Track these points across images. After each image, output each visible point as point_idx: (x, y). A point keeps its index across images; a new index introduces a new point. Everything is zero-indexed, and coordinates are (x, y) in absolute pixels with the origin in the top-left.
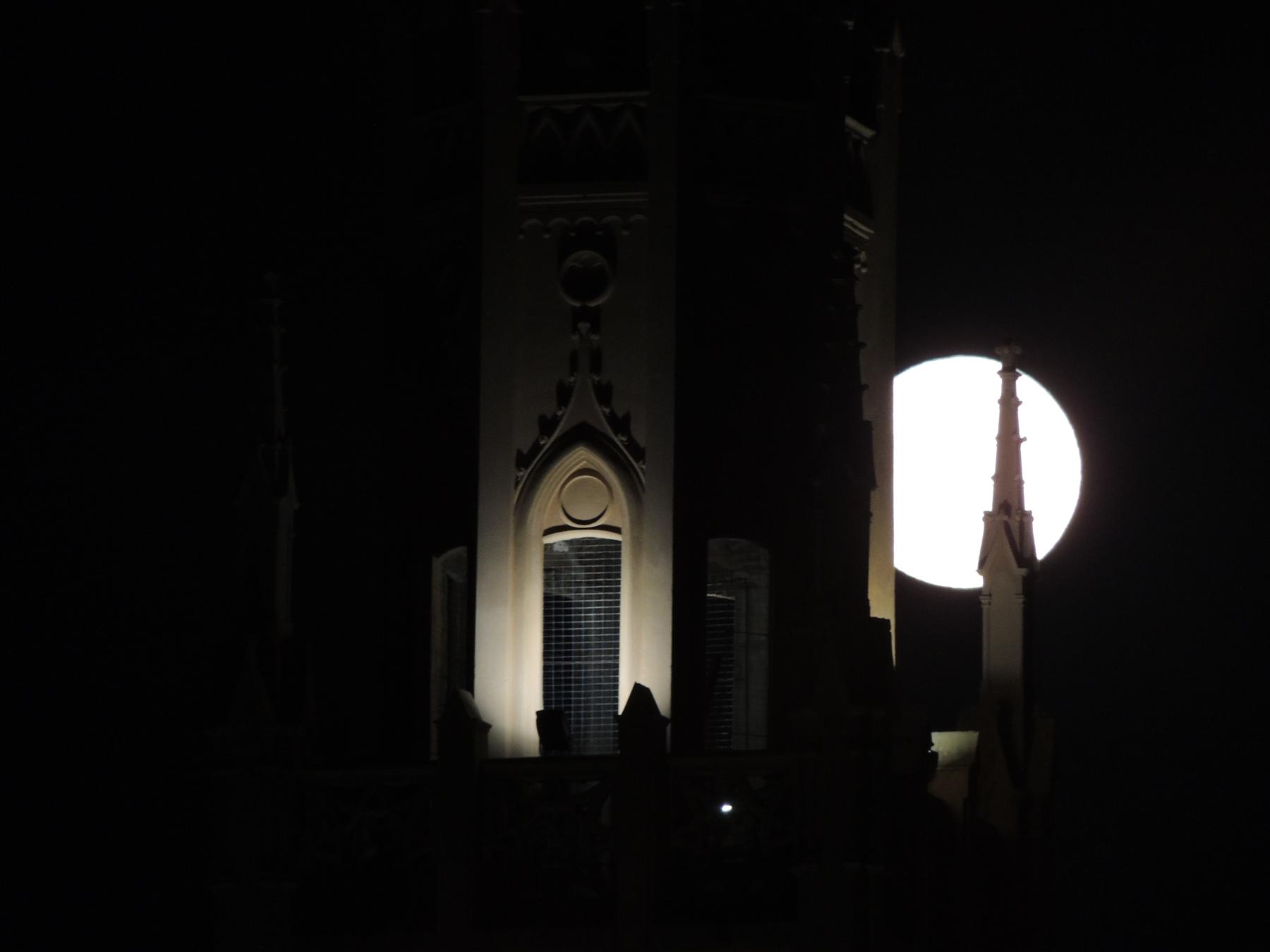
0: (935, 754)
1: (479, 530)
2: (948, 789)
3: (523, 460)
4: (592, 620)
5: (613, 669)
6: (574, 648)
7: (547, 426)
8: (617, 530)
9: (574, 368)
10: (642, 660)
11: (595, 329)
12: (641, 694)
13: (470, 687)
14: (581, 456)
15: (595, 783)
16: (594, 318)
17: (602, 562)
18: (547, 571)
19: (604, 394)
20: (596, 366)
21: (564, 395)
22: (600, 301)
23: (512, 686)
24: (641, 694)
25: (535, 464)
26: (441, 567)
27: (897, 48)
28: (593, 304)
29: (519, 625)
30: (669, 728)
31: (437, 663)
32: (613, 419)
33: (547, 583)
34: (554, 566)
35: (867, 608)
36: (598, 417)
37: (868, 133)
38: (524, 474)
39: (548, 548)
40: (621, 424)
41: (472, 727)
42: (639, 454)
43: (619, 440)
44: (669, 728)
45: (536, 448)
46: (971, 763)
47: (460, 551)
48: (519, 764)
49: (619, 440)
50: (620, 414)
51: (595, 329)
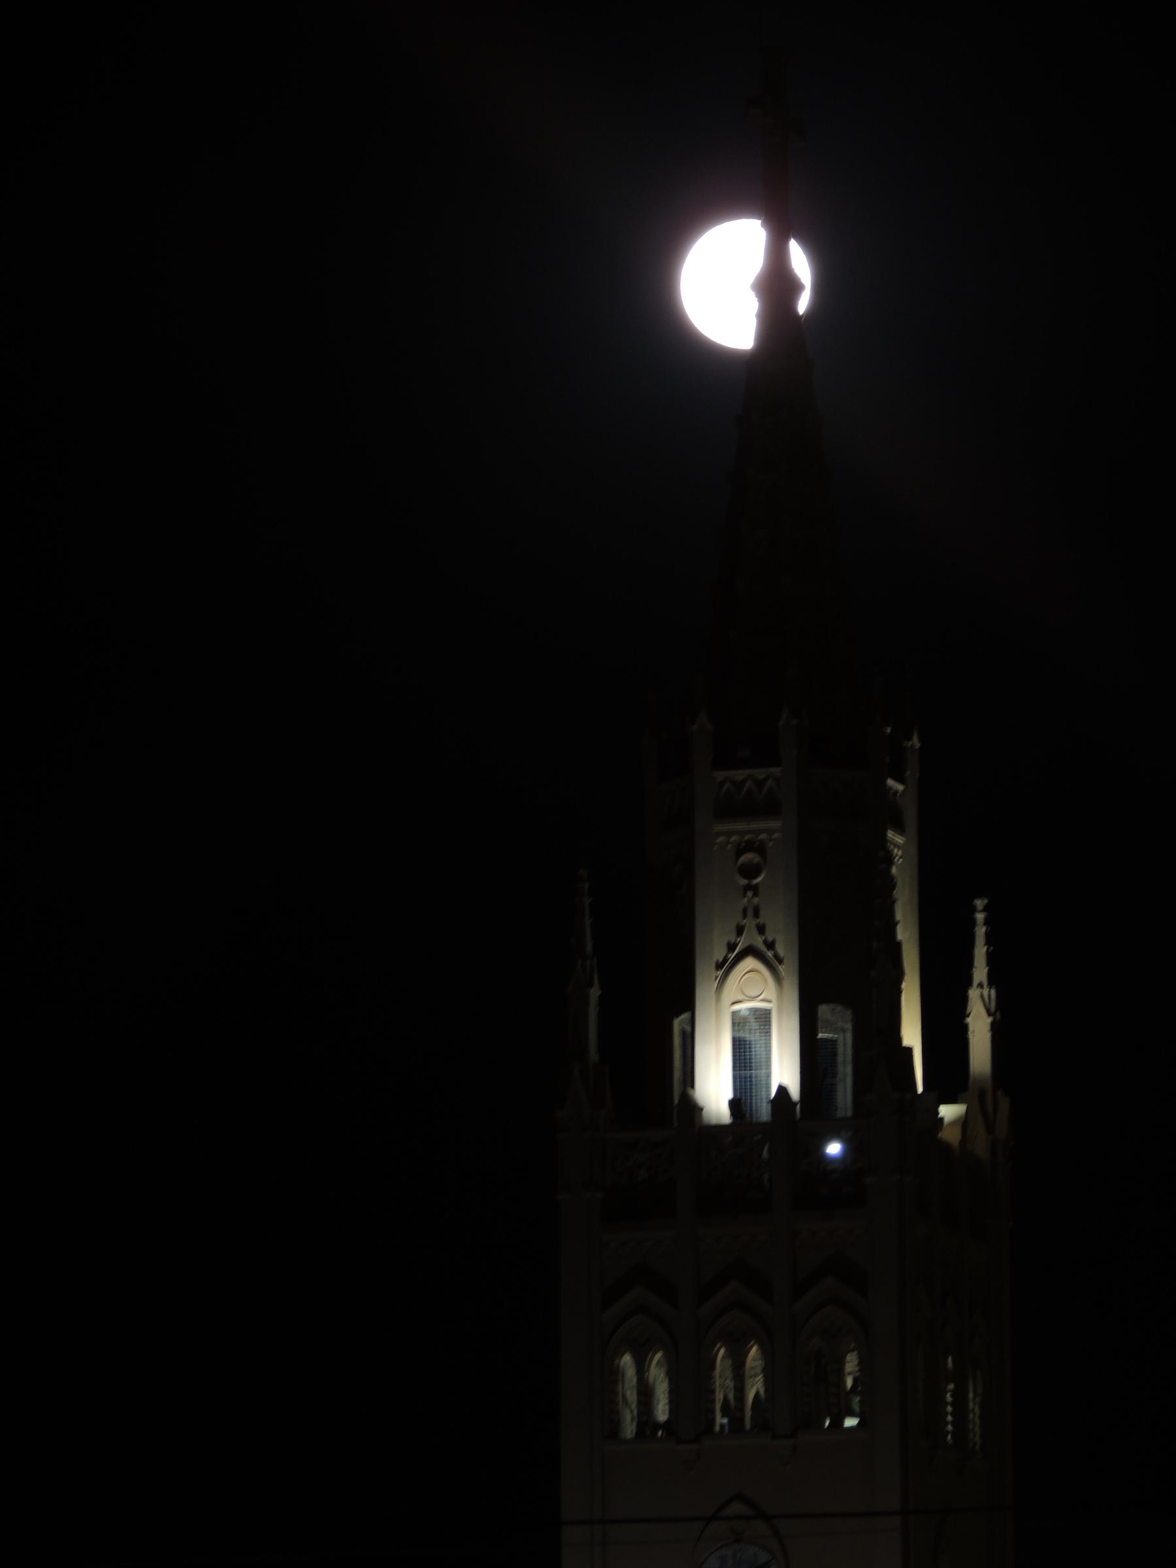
0: (942, 1119)
1: (699, 928)
2: (951, 1136)
3: (719, 966)
4: (758, 1050)
5: (769, 1076)
6: (747, 1062)
7: (731, 947)
8: (770, 1001)
9: (745, 916)
10: (784, 1071)
11: (756, 894)
12: (782, 1090)
13: (693, 1086)
14: (750, 963)
15: (950, 1359)
16: (755, 890)
17: (763, 1018)
18: (734, 1024)
19: (761, 929)
20: (756, 914)
21: (740, 931)
22: (759, 879)
23: (714, 1088)
24: (782, 1090)
25: (725, 967)
26: (678, 1024)
27: (915, 742)
28: (755, 882)
29: (718, 1052)
30: (798, 1107)
31: (677, 1074)
32: (765, 942)
33: (733, 1030)
34: (738, 1022)
35: (900, 1040)
36: (758, 942)
37: (900, 787)
38: (720, 973)
39: (734, 1014)
40: (771, 946)
41: (692, 1109)
42: (780, 961)
43: (770, 954)
44: (798, 1107)
45: (725, 960)
46: (964, 1122)
47: (685, 1016)
48: (720, 1128)
49: (770, 954)
50: (770, 939)
51: (756, 894)
